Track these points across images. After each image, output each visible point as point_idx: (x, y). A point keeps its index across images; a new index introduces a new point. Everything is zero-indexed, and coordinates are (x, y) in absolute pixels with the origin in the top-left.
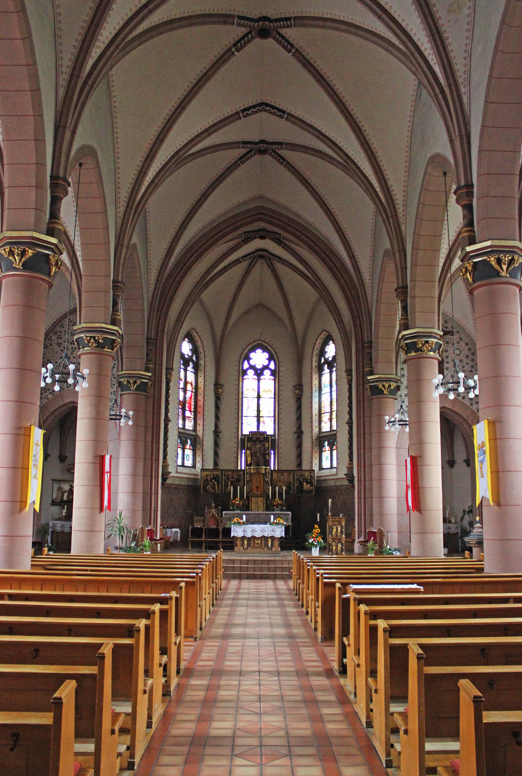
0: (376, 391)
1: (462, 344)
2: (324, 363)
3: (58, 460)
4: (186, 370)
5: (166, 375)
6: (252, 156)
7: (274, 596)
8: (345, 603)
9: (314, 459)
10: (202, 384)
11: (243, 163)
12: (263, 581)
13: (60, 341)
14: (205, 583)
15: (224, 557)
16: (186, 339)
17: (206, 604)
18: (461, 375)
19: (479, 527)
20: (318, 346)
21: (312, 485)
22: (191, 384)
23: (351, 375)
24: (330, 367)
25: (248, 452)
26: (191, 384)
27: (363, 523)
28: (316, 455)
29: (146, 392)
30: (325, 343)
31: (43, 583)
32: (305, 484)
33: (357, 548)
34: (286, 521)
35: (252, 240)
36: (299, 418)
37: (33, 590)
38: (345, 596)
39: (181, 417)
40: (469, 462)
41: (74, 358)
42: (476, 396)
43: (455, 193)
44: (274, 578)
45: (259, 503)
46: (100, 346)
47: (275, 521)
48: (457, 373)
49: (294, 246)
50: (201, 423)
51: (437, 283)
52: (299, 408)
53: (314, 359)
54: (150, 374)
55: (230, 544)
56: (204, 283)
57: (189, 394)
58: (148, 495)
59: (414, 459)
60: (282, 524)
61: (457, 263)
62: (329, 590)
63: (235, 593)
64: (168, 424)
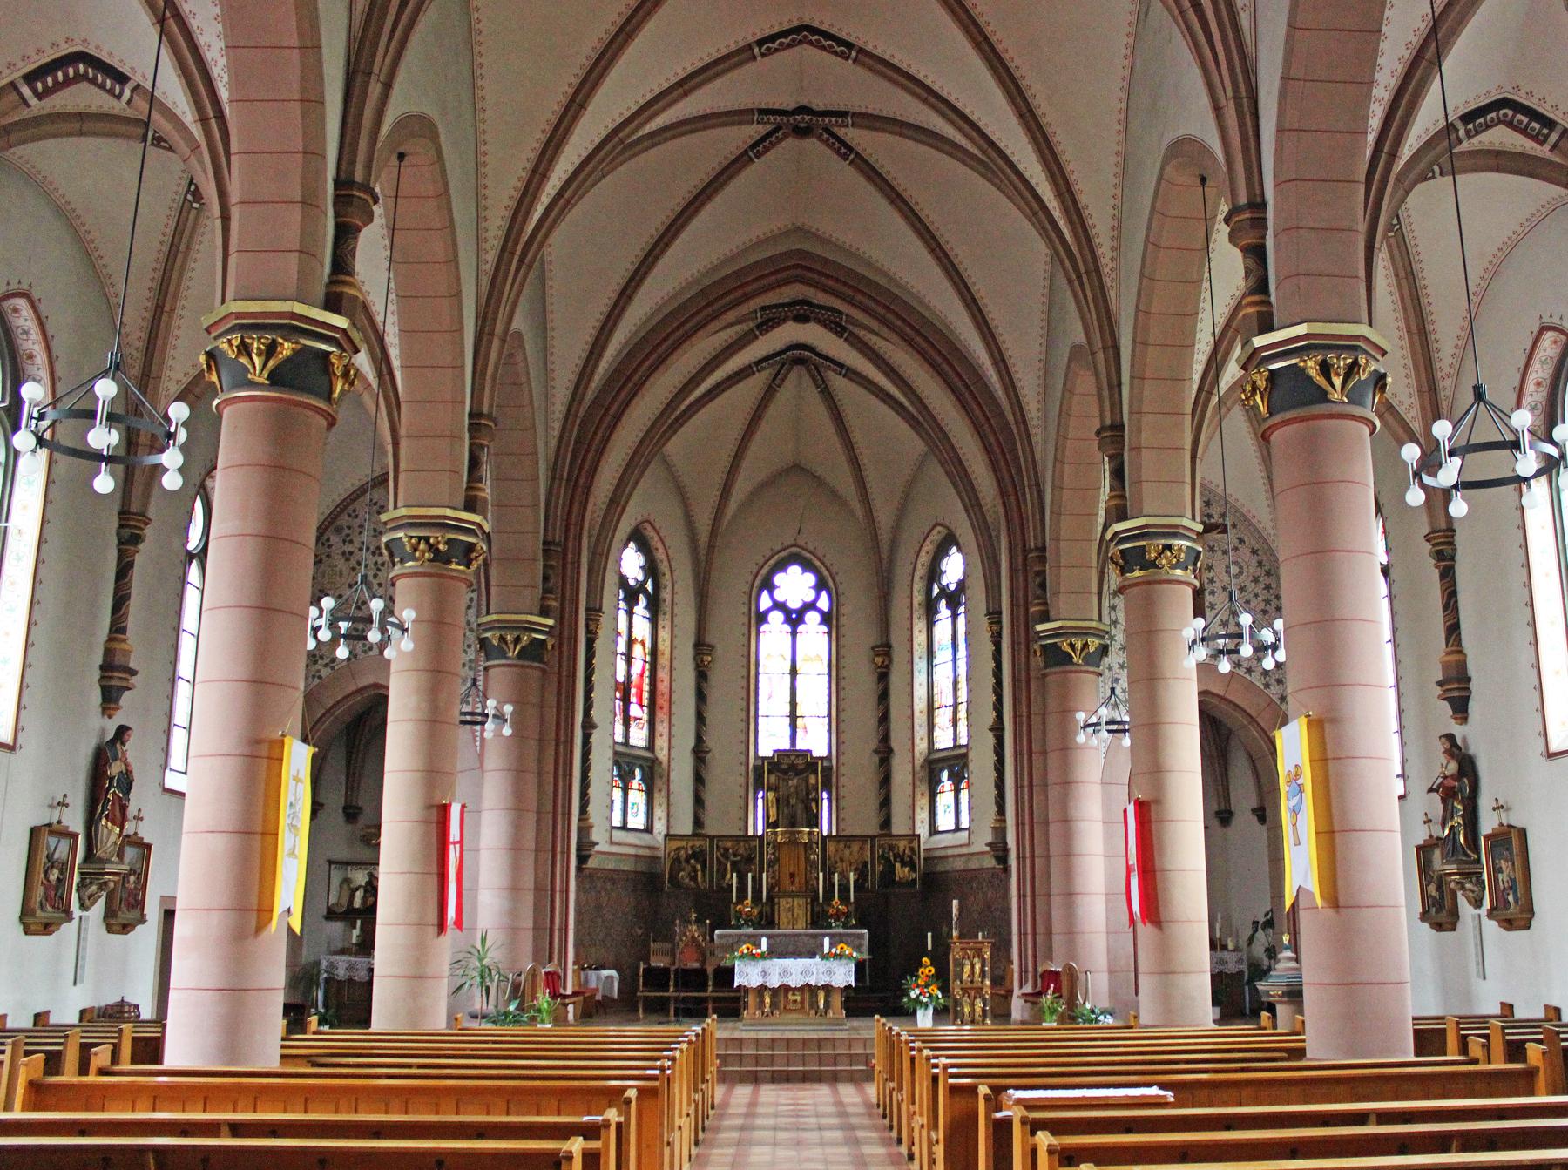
0: (1056, 657)
1: (1245, 552)
2: (939, 597)
3: (341, 818)
4: (630, 613)
5: (587, 626)
6: (779, 140)
7: (834, 1121)
8: (1002, 1130)
9: (918, 810)
10: (668, 643)
11: (758, 156)
12: (807, 1085)
13: (348, 548)
14: (680, 1092)
15: (721, 1033)
16: (632, 545)
17: (682, 1139)
18: (1246, 619)
19: (1290, 959)
20: (925, 558)
21: (913, 868)
22: (643, 643)
23: (999, 622)
24: (953, 604)
25: (771, 795)
26: (643, 643)
27: (1030, 952)
28: (923, 802)
29: (541, 661)
30: (941, 552)
31: (308, 1097)
32: (898, 865)
33: (1018, 1008)
34: (858, 948)
35: (778, 324)
36: (884, 719)
37: (285, 1111)
38: (999, 1115)
39: (619, 718)
40: (1266, 813)
41: (380, 585)
42: (1279, 665)
43: (1227, 221)
44: (834, 1079)
46: (439, 557)
48: (1235, 614)
49: (873, 340)
51: (1188, 419)
52: (884, 697)
54: (551, 622)
55: (732, 1003)
56: (671, 419)
58: (546, 895)
59: (1142, 808)
60: (850, 957)
61: (1232, 372)
62: (962, 1102)
63: (747, 1115)
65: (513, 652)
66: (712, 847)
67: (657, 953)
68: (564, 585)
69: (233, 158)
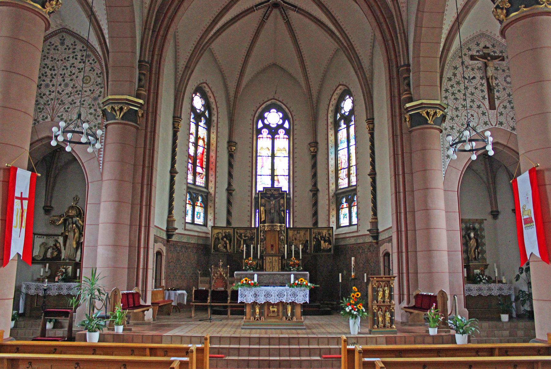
2: (340, 119)
4: (197, 126)
9: (331, 217)
10: (215, 140)
20: (333, 102)
22: (203, 139)
26: (203, 139)
28: (334, 213)
29: (136, 123)
30: (341, 99)
32: (322, 242)
41: (53, 85)
45: (274, 264)
47: (297, 282)
50: (213, 180)
51: (438, 60)
53: (329, 115)
54: (141, 101)
55: (239, 310)
57: (200, 150)
60: (306, 286)
64: (174, 176)
65: (119, 115)
66: (234, 233)
67: (202, 282)
68: (150, 84)
69: (110, 54)
